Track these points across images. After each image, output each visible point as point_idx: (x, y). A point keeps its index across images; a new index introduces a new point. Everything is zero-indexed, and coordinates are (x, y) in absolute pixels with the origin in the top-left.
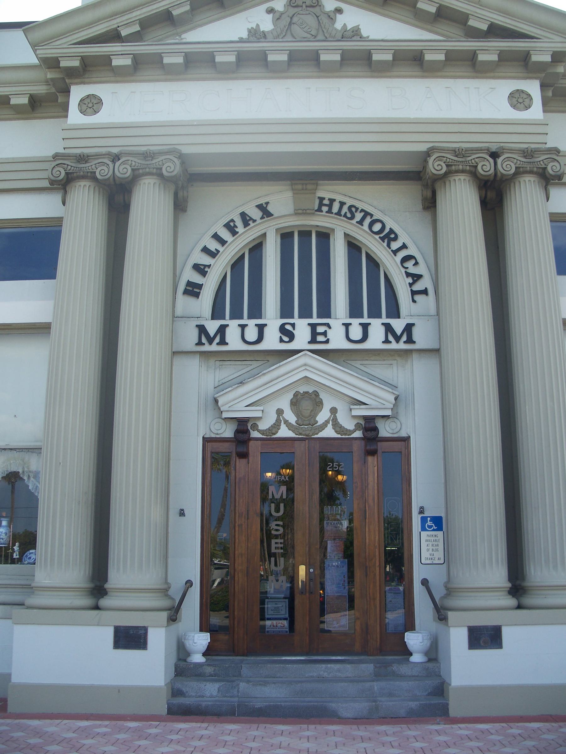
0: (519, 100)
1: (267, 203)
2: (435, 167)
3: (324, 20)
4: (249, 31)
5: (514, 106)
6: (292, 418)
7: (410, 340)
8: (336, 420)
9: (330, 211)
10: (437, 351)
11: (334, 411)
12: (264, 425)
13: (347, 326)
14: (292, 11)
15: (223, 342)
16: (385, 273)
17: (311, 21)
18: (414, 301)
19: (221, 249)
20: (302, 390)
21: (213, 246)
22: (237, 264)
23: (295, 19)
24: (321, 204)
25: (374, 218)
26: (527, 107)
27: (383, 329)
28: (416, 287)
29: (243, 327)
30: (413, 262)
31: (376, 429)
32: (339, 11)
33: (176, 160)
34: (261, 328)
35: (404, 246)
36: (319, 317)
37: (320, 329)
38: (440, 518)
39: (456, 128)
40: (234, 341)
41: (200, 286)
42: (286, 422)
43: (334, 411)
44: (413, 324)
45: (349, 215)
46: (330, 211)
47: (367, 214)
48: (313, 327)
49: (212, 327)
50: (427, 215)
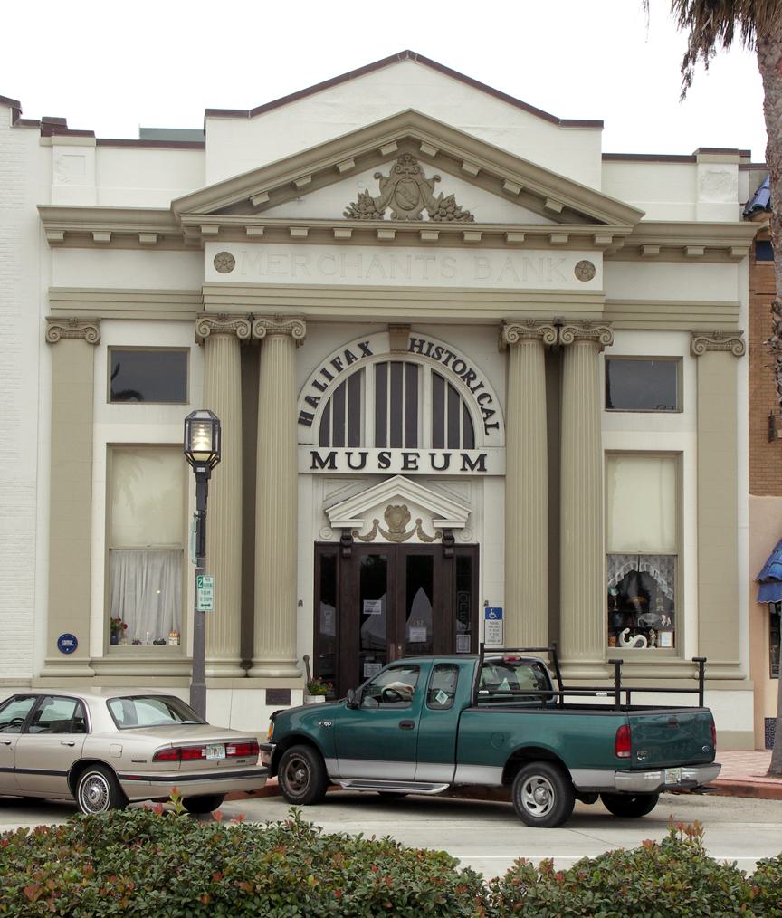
0: (584, 271)
1: (367, 343)
2: (509, 335)
3: (424, 187)
4: (360, 196)
5: (579, 277)
6: (386, 528)
7: (482, 468)
8: (420, 531)
9: (420, 352)
10: (504, 476)
11: (419, 522)
12: (363, 533)
13: (433, 455)
14: (397, 177)
15: (333, 466)
16: (464, 403)
17: (412, 188)
18: (487, 433)
19: (329, 383)
20: (394, 504)
21: (322, 380)
22: (339, 392)
23: (399, 188)
24: (413, 345)
25: (457, 359)
26: (590, 277)
27: (461, 459)
28: (488, 422)
29: (349, 454)
30: (488, 399)
31: (452, 538)
32: (437, 179)
33: (300, 322)
34: (364, 455)
35: (481, 385)
36: (407, 447)
37: (411, 458)
38: (501, 609)
39: (529, 298)
40: (341, 466)
41: (312, 416)
42: (381, 530)
43: (419, 522)
44: (486, 455)
45: (436, 356)
46: (420, 352)
47: (451, 355)
48: (406, 456)
49: (324, 453)
50: (503, 357)
